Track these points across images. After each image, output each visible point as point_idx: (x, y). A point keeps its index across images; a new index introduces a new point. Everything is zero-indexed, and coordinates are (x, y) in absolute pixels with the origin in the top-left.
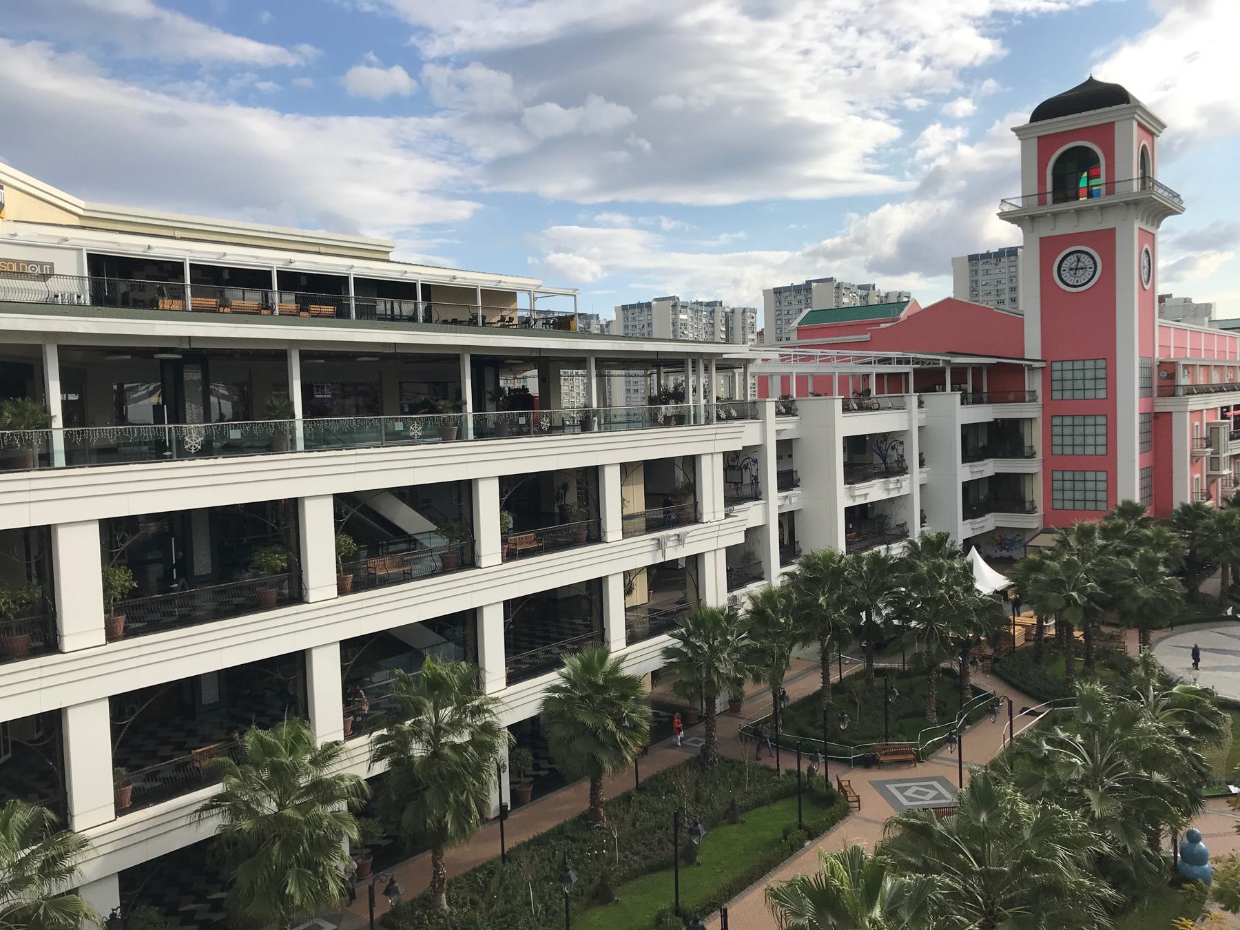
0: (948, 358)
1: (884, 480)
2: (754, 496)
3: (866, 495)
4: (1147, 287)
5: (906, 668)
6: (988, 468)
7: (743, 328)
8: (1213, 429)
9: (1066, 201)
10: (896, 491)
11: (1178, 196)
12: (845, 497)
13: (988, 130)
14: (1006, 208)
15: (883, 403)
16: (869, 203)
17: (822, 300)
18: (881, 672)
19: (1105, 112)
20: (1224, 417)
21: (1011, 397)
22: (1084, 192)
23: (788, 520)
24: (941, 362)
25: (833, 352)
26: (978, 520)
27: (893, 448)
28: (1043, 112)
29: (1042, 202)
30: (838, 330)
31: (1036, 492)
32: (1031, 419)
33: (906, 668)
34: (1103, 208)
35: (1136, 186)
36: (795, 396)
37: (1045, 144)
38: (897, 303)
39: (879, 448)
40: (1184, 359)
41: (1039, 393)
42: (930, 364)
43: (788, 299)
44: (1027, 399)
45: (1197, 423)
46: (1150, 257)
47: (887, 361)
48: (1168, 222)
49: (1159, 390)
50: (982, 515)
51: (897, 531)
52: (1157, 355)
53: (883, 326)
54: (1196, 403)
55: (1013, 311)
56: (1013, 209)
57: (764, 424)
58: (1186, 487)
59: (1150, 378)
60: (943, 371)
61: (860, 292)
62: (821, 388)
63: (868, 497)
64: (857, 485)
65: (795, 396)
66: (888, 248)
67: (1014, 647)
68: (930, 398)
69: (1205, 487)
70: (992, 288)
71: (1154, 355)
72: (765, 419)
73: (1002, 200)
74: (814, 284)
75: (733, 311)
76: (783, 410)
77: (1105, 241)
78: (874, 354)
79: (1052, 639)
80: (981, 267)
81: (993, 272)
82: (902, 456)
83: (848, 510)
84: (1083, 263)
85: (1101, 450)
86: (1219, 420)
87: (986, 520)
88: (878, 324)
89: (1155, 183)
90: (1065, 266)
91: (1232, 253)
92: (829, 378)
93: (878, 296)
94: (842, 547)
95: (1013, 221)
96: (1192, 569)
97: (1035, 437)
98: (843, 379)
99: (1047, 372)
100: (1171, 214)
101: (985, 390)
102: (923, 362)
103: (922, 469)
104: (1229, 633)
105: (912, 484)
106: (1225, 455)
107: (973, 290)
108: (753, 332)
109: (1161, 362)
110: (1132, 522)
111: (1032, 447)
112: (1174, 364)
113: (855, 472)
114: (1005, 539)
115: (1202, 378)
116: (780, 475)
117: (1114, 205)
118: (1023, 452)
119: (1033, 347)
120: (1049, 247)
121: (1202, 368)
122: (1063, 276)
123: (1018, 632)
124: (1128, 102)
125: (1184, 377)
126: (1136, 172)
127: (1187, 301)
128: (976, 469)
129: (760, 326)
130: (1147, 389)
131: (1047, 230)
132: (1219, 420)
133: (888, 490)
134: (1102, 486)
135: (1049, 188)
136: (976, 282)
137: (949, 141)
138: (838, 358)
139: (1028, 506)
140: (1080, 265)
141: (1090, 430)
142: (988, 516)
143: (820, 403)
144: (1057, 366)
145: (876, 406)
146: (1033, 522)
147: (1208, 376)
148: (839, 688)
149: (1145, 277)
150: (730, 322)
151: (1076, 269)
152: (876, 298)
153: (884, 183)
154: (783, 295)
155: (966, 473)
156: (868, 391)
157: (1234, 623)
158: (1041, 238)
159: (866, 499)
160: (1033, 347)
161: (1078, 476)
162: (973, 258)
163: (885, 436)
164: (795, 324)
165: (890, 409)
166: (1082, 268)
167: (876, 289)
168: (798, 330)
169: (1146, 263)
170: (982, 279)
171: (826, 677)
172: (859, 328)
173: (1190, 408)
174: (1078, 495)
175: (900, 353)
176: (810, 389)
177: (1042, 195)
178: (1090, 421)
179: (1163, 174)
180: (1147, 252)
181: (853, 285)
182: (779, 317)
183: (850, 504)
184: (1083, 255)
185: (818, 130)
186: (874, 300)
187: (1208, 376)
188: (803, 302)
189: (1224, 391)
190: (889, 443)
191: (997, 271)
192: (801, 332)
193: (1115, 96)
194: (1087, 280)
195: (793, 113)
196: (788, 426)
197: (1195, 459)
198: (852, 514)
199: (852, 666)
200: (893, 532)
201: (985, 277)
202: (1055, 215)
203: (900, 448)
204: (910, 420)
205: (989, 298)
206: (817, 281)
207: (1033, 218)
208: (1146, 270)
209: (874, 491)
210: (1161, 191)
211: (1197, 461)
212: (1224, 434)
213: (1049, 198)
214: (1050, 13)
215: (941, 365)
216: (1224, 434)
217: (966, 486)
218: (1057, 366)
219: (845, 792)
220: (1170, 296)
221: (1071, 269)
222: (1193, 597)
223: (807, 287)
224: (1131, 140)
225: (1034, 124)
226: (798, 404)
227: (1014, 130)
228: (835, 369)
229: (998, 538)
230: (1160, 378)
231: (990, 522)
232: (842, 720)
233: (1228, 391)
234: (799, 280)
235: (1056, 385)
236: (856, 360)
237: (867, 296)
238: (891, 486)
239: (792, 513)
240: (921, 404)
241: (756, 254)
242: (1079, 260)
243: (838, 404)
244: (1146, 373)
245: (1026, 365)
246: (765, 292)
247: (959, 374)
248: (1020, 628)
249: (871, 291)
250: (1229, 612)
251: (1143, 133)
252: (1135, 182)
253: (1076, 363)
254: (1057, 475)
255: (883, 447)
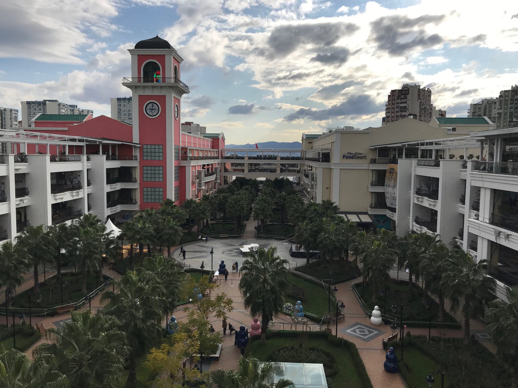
0: (101, 141)
1: (71, 192)
2: (3, 200)
3: (62, 198)
4: (177, 119)
5: (76, 272)
6: (118, 186)
7: (11, 118)
8: (199, 172)
9: (148, 82)
10: (61, 200)
11: (187, 87)
12: (51, 200)
13: (119, 47)
14: (126, 81)
15: (70, 159)
16: (69, 68)
17: (51, 110)
18: (64, 275)
19: (162, 50)
20: (203, 168)
21: (127, 158)
22: (155, 79)
23: (21, 212)
24: (98, 142)
25: (47, 135)
26: (113, 208)
27: (76, 178)
28: (140, 45)
29: (139, 81)
30: (55, 124)
31: (137, 196)
32: (135, 167)
33: (76, 272)
34: (161, 87)
35: (173, 81)
36: (26, 153)
37: (141, 58)
38: (82, 115)
39: (70, 178)
40: (190, 147)
41: (138, 157)
42: (93, 143)
43: (34, 107)
44: (133, 159)
45: (194, 170)
46: (178, 107)
47: (74, 140)
48: (184, 95)
49: (181, 158)
50: (115, 206)
51: (77, 213)
52: (181, 145)
53: (74, 124)
54: (193, 163)
55: (130, 123)
56: (129, 82)
57: (8, 166)
58: (190, 194)
59: (179, 153)
60: (98, 146)
61: (70, 108)
62: (42, 150)
63: (63, 199)
64: (57, 194)
65: (26, 153)
66: (79, 91)
67: (122, 258)
68: (93, 157)
69: (197, 193)
70: (126, 112)
71: (180, 145)
72: (8, 163)
73: (124, 78)
74: (47, 102)
75: (5, 110)
76: (19, 160)
77: (162, 99)
78: (67, 137)
79: (138, 253)
80: (122, 103)
81: (127, 106)
82: (80, 181)
83: (54, 206)
84: (155, 107)
85: (161, 180)
86: (202, 170)
87: (117, 208)
88: (73, 123)
89: (179, 81)
90: (148, 107)
91: (209, 110)
92: (45, 146)
93: (78, 111)
94: (50, 223)
95: (128, 87)
96: (188, 224)
97: (137, 174)
98: (53, 147)
99: (141, 149)
100: (185, 93)
101: (117, 154)
102: (90, 141)
103: (89, 187)
104: (199, 245)
105: (84, 193)
106: (203, 182)
107: (119, 112)
108: (16, 121)
109: (182, 147)
110: (170, 207)
111: (135, 178)
112: (186, 149)
113: (56, 189)
114: (125, 215)
115: (196, 154)
116: (17, 190)
117: (165, 87)
118: (132, 180)
119: (136, 139)
120: (142, 99)
121: (196, 151)
122: (147, 111)
123: (124, 251)
124: (170, 48)
125: (190, 153)
126: (173, 75)
127: (198, 125)
128: (113, 187)
129: (20, 119)
130: (177, 158)
131: (141, 92)
132: (202, 170)
133: (73, 196)
134: (161, 193)
135: (142, 76)
136: (120, 109)
137: (100, 48)
138: (49, 137)
139: (134, 201)
140: (154, 108)
141: (157, 172)
142: (118, 206)
143: (40, 157)
144: (145, 146)
145: (67, 159)
146: (136, 208)
147: (198, 153)
148: (43, 285)
149: (176, 115)
150: (3, 115)
151: (152, 109)
152: (78, 111)
153: (78, 61)
154: (32, 105)
155: (108, 188)
156: (65, 153)
157: (202, 241)
158: (139, 95)
159: (62, 200)
160: (136, 139)
161: (153, 189)
162: (119, 99)
163: (72, 173)
164: (33, 120)
165: (74, 161)
166: (154, 109)
167: (78, 107)
168: (35, 122)
169: (176, 110)
170: (123, 109)
171: (36, 279)
172: (64, 124)
173: (192, 165)
174: (153, 197)
175: (80, 137)
176: (37, 151)
177: (139, 78)
178: (157, 168)
179: (183, 78)
180: (177, 106)
181: (67, 105)
182: (30, 115)
183: (54, 202)
184: (154, 104)
185: (47, 31)
186: (76, 113)
187: (198, 153)
188: (42, 109)
189: (203, 159)
190: (74, 175)
191: (129, 106)
192: (36, 123)
193: (166, 45)
194: (156, 114)
195: (34, 20)
196: (23, 168)
197: (193, 183)
198: (55, 207)
199: (51, 274)
200: (75, 214)
201: (124, 108)
202: (144, 87)
203: (79, 178)
204: (83, 166)
205: (125, 116)
206: (49, 101)
207: (136, 87)
208: (177, 113)
209: (66, 197)
210: (181, 84)
211: (194, 184)
212: (203, 174)
213: (142, 80)
214: (146, 5)
215: (98, 143)
216: (203, 174)
217: (109, 194)
218: (145, 146)
219: (39, 329)
220: (193, 123)
221: (150, 109)
222: (189, 234)
223: (44, 103)
224: (170, 63)
225: (136, 49)
226: (28, 157)
227: (129, 50)
228: (49, 142)
229: (122, 215)
230: (182, 153)
231: (119, 208)
232: (38, 298)
233: (205, 159)
234: (40, 99)
235: (145, 154)
236: (59, 139)
237: (73, 110)
238: (74, 194)
239: (25, 208)
240: (88, 159)
241: (19, 83)
242: (153, 106)
243: (48, 158)
244: (177, 151)
245: (133, 145)
246: (22, 103)
247: (106, 148)
248: (126, 250)
249: (75, 108)
250: (200, 237)
251: (175, 61)
252: (172, 79)
253: (152, 146)
254: (145, 189)
255: (71, 177)
